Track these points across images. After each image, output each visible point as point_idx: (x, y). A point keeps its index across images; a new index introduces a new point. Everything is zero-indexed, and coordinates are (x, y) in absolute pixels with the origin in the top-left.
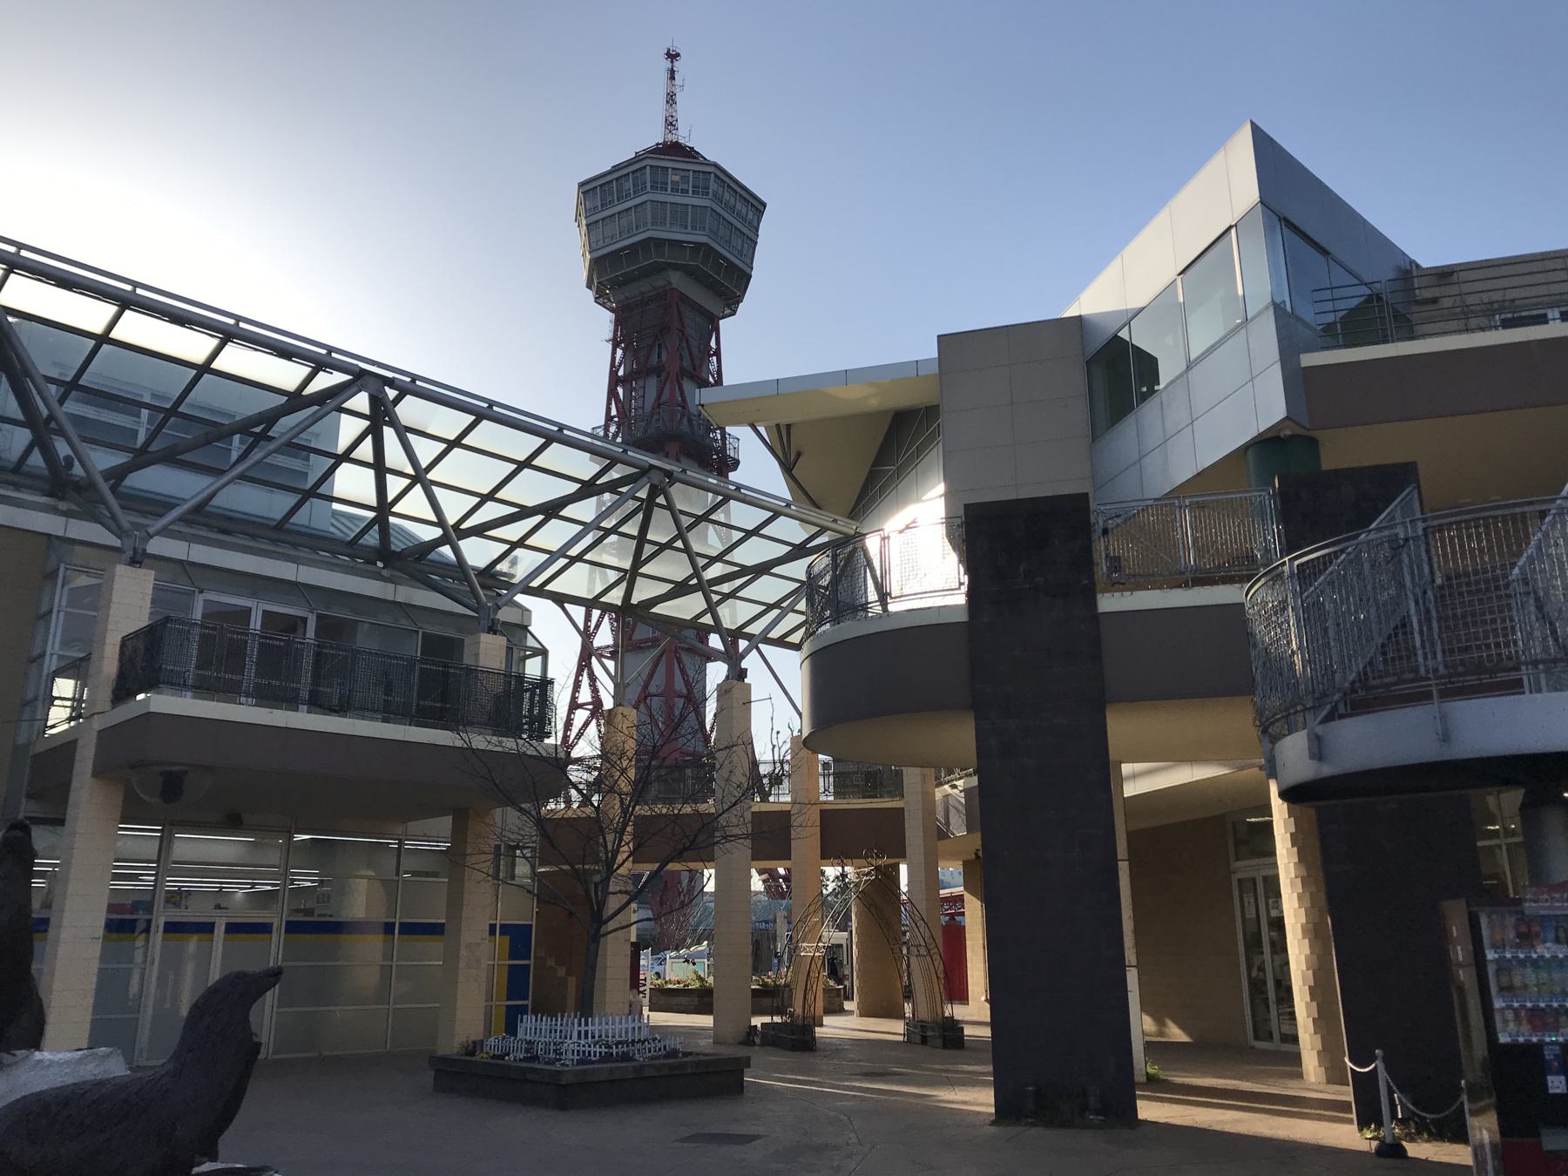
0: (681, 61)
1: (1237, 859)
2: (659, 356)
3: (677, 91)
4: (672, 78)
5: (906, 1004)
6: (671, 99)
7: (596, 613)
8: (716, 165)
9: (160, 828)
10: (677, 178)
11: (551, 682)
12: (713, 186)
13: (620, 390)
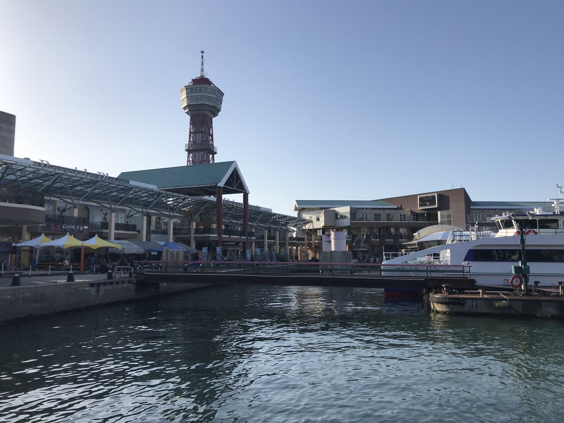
4: (202, 58)
5: (383, 289)
6: (202, 64)
7: (200, 130)
8: (218, 88)
10: (209, 90)
11: (187, 150)
12: (217, 92)
13: (192, 135)
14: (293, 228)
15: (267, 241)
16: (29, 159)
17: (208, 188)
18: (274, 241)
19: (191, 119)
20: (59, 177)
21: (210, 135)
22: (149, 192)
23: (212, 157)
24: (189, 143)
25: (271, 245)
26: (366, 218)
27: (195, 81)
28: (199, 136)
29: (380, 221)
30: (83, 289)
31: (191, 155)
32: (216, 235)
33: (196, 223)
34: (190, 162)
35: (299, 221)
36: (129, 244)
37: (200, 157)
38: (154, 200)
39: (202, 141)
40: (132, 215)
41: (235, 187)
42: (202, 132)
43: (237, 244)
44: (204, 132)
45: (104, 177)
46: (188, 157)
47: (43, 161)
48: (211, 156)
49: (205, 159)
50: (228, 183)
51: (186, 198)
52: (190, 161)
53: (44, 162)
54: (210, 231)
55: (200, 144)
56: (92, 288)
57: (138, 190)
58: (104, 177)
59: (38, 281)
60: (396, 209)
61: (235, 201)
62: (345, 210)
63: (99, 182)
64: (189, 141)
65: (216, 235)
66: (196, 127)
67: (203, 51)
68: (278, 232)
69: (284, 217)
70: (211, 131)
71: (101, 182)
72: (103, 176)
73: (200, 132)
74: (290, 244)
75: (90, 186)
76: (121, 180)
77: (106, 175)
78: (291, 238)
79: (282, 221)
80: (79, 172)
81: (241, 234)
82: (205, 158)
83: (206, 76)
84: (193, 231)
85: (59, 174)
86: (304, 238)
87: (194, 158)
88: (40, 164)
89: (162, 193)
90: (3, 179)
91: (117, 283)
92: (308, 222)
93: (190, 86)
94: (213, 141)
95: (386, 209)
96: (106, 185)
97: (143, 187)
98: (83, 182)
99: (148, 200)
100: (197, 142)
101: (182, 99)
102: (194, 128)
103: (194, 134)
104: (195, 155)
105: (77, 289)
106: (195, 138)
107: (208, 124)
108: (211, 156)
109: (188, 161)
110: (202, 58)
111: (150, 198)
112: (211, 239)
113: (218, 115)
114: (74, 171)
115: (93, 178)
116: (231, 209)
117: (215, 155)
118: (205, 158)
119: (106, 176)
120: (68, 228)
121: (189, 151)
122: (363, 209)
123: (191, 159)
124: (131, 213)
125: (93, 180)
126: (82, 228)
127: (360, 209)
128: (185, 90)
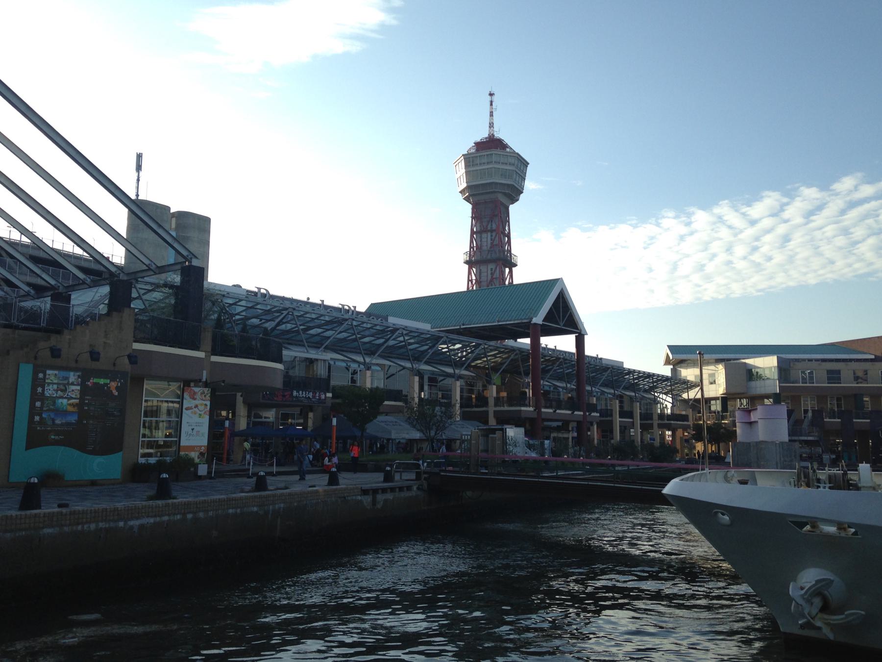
0: (495, 97)
1: (177, 441)
2: (492, 225)
3: (494, 110)
4: (491, 104)
6: (491, 114)
7: (489, 228)
8: (518, 154)
9: (422, 611)
11: (466, 262)
13: (475, 236)
14: (664, 397)
15: (617, 420)
16: (240, 287)
17: (515, 327)
18: (631, 420)
19: (473, 209)
20: (288, 314)
21: (505, 235)
22: (422, 336)
23: (509, 272)
24: (470, 250)
25: (625, 427)
26: (811, 378)
27: (479, 146)
28: (486, 237)
29: (840, 383)
30: (354, 497)
31: (474, 270)
32: (531, 409)
33: (497, 388)
34: (472, 283)
35: (675, 384)
36: (396, 422)
37: (489, 272)
38: (428, 349)
39: (492, 245)
40: (394, 374)
41: (562, 325)
42: (492, 231)
43: (565, 426)
44: (495, 230)
45: (350, 313)
46: (469, 273)
47: (260, 289)
48: (507, 270)
49: (498, 276)
50: (549, 317)
51: (481, 344)
52: (471, 281)
53: (263, 291)
54: (521, 399)
55: (489, 251)
56: (366, 497)
57: (405, 332)
58: (350, 313)
59: (234, 474)
60: (871, 360)
61: (557, 348)
62: (767, 364)
63: (346, 320)
64: (471, 247)
65: (531, 409)
66: (481, 223)
67: (492, 92)
68: (638, 404)
69: (649, 376)
70: (507, 228)
71: (350, 320)
72: (348, 311)
73: (489, 231)
74: (661, 426)
75: (334, 328)
76: (376, 316)
77: (352, 308)
78: (662, 416)
79: (644, 384)
80: (314, 305)
81: (573, 404)
82: (497, 274)
83: (497, 135)
84: (491, 402)
85: (290, 310)
86: (688, 416)
87: (479, 275)
88: (255, 294)
89: (442, 337)
90: (276, 330)
91: (401, 489)
92: (694, 386)
93: (471, 154)
94: (510, 245)
95: (851, 360)
96: (300, 316)
97: (424, 330)
98: (323, 322)
99: (419, 349)
100: (485, 248)
101: (458, 178)
102: (478, 225)
103: (479, 235)
104: (480, 270)
105: (345, 497)
106: (481, 241)
107: (502, 216)
108: (507, 270)
109: (469, 280)
110: (491, 104)
111: (379, 338)
112: (523, 415)
113: (518, 200)
114: (307, 303)
115: (335, 314)
116: (554, 362)
117: (513, 269)
118: (497, 274)
119: (353, 311)
120: (303, 397)
121: (470, 263)
122: (804, 360)
123: (474, 278)
124: (392, 371)
125: (338, 318)
126: (323, 397)
127: (797, 360)
128: (463, 161)
